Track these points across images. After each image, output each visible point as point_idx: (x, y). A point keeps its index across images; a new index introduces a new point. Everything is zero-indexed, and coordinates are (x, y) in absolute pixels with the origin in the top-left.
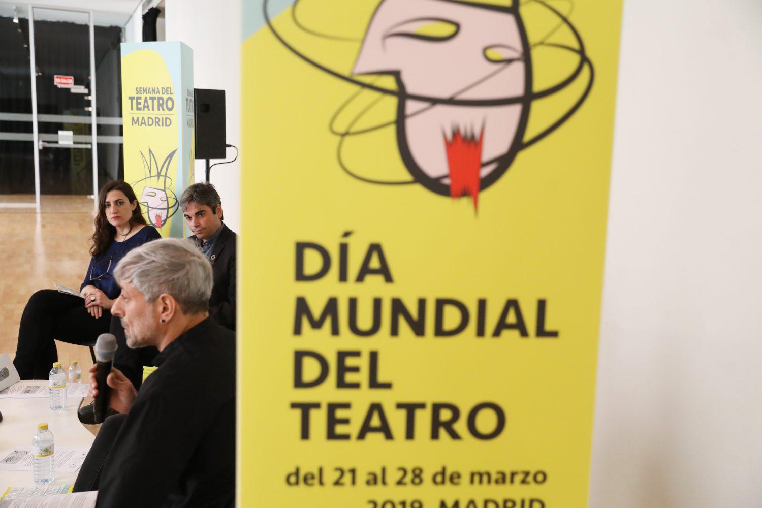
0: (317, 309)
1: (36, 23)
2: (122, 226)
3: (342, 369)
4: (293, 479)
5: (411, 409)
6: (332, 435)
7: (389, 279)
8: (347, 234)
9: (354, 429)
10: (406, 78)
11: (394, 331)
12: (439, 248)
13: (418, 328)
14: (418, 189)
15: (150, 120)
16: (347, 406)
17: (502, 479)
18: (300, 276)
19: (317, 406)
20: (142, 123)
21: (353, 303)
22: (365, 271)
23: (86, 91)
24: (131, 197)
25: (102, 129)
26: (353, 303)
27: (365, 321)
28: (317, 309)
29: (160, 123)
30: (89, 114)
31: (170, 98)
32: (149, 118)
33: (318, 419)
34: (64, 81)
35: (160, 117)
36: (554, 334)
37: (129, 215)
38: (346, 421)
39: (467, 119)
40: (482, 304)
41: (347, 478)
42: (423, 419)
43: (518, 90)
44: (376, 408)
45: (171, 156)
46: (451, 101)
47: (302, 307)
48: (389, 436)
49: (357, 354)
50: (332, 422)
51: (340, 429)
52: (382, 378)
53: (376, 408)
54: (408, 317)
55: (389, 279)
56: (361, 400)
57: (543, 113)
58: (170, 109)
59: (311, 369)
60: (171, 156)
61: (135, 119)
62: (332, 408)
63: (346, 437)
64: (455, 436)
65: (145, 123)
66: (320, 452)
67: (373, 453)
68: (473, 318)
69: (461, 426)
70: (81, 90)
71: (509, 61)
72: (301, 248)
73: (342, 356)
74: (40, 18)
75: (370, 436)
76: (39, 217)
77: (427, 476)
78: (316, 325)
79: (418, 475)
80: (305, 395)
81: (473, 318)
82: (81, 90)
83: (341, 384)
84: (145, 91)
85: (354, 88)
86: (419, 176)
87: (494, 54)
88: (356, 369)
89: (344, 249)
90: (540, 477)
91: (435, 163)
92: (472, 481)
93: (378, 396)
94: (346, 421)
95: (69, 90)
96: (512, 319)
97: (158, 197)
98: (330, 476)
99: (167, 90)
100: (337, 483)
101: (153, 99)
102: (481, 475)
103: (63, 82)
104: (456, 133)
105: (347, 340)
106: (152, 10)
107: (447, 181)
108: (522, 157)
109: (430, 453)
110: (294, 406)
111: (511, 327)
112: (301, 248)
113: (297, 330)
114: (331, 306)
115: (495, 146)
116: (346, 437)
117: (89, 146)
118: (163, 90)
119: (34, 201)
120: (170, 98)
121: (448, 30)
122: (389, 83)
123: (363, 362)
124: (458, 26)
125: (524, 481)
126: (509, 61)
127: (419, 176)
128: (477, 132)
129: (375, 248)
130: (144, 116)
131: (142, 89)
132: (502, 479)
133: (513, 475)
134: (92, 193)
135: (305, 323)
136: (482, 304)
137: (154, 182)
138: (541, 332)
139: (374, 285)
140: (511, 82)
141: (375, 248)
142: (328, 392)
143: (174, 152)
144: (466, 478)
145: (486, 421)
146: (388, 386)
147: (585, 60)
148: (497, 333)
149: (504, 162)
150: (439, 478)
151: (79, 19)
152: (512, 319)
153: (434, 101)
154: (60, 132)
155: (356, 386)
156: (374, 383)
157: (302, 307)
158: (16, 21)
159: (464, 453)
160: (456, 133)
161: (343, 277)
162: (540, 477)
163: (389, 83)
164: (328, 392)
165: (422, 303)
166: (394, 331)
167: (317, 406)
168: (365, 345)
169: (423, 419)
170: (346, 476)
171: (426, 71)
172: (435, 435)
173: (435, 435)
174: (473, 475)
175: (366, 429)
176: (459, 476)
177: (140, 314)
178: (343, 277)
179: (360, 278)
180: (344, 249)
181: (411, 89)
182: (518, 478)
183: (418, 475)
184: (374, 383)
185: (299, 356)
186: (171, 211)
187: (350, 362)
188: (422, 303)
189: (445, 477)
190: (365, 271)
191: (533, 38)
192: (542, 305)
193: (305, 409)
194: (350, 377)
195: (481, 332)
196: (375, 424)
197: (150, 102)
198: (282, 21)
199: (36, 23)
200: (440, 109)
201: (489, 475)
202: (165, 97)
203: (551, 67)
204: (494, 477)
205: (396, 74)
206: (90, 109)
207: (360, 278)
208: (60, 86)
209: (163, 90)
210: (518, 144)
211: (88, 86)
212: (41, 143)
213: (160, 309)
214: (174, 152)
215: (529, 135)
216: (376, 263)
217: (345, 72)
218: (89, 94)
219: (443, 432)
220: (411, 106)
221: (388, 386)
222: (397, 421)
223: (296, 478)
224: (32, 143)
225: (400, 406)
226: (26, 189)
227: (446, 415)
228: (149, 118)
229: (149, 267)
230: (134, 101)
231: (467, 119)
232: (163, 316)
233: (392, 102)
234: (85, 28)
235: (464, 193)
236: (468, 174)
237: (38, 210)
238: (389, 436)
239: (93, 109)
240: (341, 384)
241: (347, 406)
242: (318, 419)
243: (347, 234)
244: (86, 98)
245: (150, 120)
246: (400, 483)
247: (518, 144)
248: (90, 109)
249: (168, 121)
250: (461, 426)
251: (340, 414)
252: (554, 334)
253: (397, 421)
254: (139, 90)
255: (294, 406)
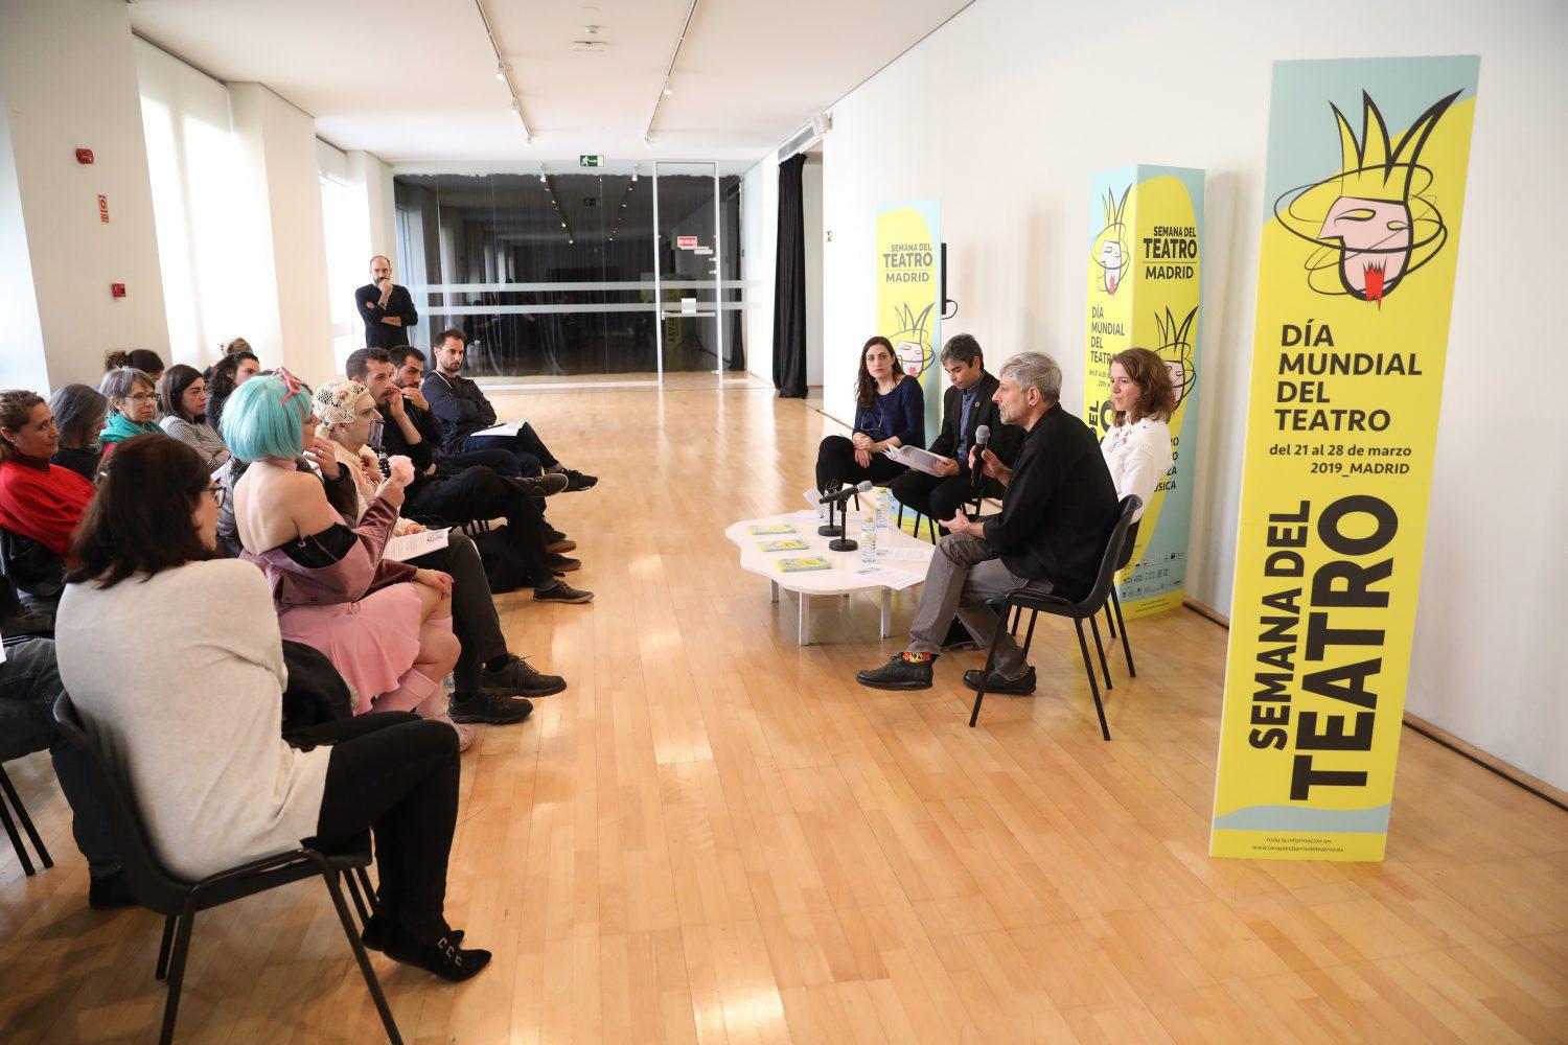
0: (1292, 361)
1: (661, 179)
2: (883, 379)
3: (1304, 392)
4: (1274, 451)
5: (1338, 413)
6: (1296, 427)
7: (1331, 344)
8: (1311, 321)
9: (1307, 424)
10: (1345, 240)
11: (1333, 372)
12: (1359, 327)
13: (1345, 370)
14: (1349, 296)
15: (1170, 271)
16: (1305, 411)
17: (1386, 452)
18: (1285, 343)
19: (1289, 411)
20: (1160, 275)
21: (1311, 356)
22: (1319, 340)
23: (711, 252)
24: (892, 352)
25: (461, 301)
26: (1311, 356)
27: (1317, 366)
28: (1292, 361)
29: (917, 278)
30: (713, 278)
31: (928, 254)
32: (1168, 268)
33: (1289, 418)
34: (687, 242)
35: (1181, 266)
36: (1419, 373)
37: (890, 369)
38: (1304, 420)
39: (1377, 260)
40: (1380, 357)
41: (1303, 450)
42: (1345, 419)
43: (1404, 243)
44: (1320, 412)
45: (928, 310)
46: (1369, 251)
47: (1285, 358)
48: (1326, 428)
49: (1312, 384)
50: (1297, 420)
51: (1300, 424)
52: (1324, 397)
53: (1320, 412)
54: (1341, 364)
55: (1331, 344)
56: (1312, 409)
57: (1418, 255)
58: (928, 265)
59: (1287, 392)
60: (928, 310)
61: (1151, 270)
62: (1297, 412)
63: (1304, 428)
64: (1362, 428)
65: (1163, 275)
66: (1290, 437)
67: (1317, 437)
68: (1376, 364)
69: (1365, 423)
70: (706, 251)
71: (1401, 229)
72: (1286, 328)
73: (1304, 384)
74: (668, 171)
75: (1316, 428)
76: (661, 394)
77: (1345, 450)
78: (1292, 368)
79: (1340, 449)
80: (1283, 406)
81: (1376, 364)
82: (706, 251)
83: (1303, 400)
84: (901, 248)
85: (1319, 246)
86: (1350, 290)
87: (1393, 226)
88: (1311, 392)
89: (1308, 329)
90: (1407, 452)
91: (1109, 287)
92: (1370, 454)
93: (1322, 406)
94: (1304, 420)
95: (693, 251)
96: (1396, 364)
97: (912, 350)
98: (1293, 450)
99: (925, 246)
100: (1297, 453)
101: (1174, 242)
102: (1374, 450)
103: (686, 243)
104: (1371, 267)
105: (1308, 377)
106: (797, 155)
107: (1364, 292)
108: (1406, 279)
109: (1347, 437)
110: (1277, 411)
111: (1319, 425)
112: (1286, 328)
113: (1281, 372)
114: (1300, 358)
115: (1391, 273)
116: (1304, 428)
117: (713, 314)
118: (1192, 252)
119: (656, 378)
120: (1192, 242)
121: (1371, 214)
122: (1337, 243)
123: (1315, 388)
124: (1374, 212)
125: (1398, 454)
126: (1401, 229)
127: (1350, 290)
128: (1382, 266)
129: (1325, 328)
130: (1156, 265)
131: (1265, 705)
132: (1386, 452)
133: (1392, 450)
134: (716, 368)
135: (1286, 367)
136: (1380, 357)
137: (909, 336)
138: (1412, 372)
139: (1324, 347)
140: (1402, 240)
141: (1325, 328)
142: (1295, 404)
143: (931, 306)
144: (1366, 452)
145: (1379, 420)
146: (1327, 401)
147: (1442, 226)
148: (1387, 373)
149: (1396, 282)
150: (1352, 452)
151: (696, 171)
152: (1396, 364)
153: (1360, 251)
154: (683, 300)
155: (1310, 401)
156: (1320, 399)
157: (1285, 358)
158: (635, 179)
159: (1366, 438)
160: (1371, 267)
161: (1307, 344)
162: (1407, 452)
163: (1337, 243)
164: (1295, 404)
165: (1348, 356)
166: (1333, 372)
167: (1289, 411)
168: (1316, 379)
169: (1345, 419)
170: (1302, 449)
171: (1356, 235)
172: (1351, 428)
173: (1351, 428)
174: (1370, 450)
175: (1314, 424)
176: (1363, 450)
177: (1015, 400)
178: (1307, 344)
179: (1316, 344)
180: (1308, 329)
181: (1348, 246)
182: (1395, 452)
183: (1340, 449)
184: (1320, 399)
185: (1282, 385)
186: (926, 364)
187: (1308, 388)
188: (1348, 356)
189: (1355, 451)
190: (1319, 340)
191: (1414, 217)
192: (1413, 357)
193: (1283, 413)
194: (1307, 396)
195: (1379, 372)
196: (1320, 421)
197: (907, 258)
198: (1284, 215)
199: (721, 179)
200: (1363, 255)
201: (1379, 450)
202: (923, 253)
203: (1423, 231)
204: (1382, 451)
205: (1341, 238)
206: (715, 272)
207: (1316, 344)
208: (683, 248)
209: (1192, 252)
210: (1404, 272)
211: (713, 247)
212: (663, 313)
213: (1029, 398)
214: (931, 306)
215: (1410, 267)
216: (1325, 335)
217: (1315, 238)
218: (714, 255)
219: (1355, 426)
220: (1348, 254)
221: (1327, 401)
222: (1331, 419)
223: (1275, 450)
224: (651, 315)
225: (1333, 412)
226: (646, 366)
227: (1357, 417)
228: (1168, 268)
229: (1025, 368)
230: (890, 259)
231: (1377, 260)
232: (1030, 403)
233: (1338, 252)
234: (707, 181)
235: (1374, 299)
236: (1377, 288)
237: (661, 388)
238: (1326, 428)
239: (717, 272)
240: (1303, 400)
241: (1305, 411)
242: (1289, 418)
243: (1311, 321)
244: (710, 259)
245: (1170, 271)
246: (1330, 454)
247: (1404, 272)
248: (715, 272)
249: (926, 277)
250: (1365, 423)
251: (1301, 416)
252: (1419, 373)
253: (1331, 419)
254: (1264, 729)
255: (1277, 411)
